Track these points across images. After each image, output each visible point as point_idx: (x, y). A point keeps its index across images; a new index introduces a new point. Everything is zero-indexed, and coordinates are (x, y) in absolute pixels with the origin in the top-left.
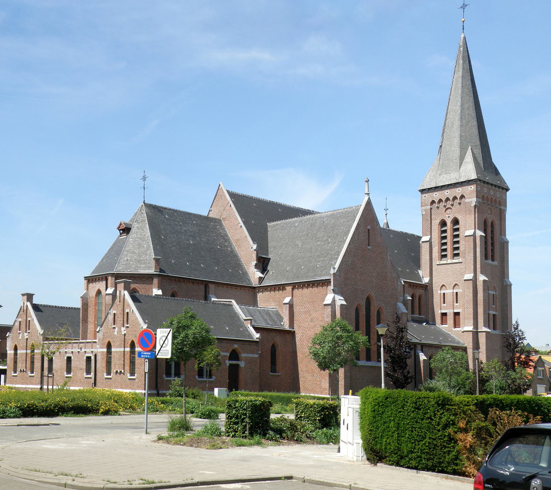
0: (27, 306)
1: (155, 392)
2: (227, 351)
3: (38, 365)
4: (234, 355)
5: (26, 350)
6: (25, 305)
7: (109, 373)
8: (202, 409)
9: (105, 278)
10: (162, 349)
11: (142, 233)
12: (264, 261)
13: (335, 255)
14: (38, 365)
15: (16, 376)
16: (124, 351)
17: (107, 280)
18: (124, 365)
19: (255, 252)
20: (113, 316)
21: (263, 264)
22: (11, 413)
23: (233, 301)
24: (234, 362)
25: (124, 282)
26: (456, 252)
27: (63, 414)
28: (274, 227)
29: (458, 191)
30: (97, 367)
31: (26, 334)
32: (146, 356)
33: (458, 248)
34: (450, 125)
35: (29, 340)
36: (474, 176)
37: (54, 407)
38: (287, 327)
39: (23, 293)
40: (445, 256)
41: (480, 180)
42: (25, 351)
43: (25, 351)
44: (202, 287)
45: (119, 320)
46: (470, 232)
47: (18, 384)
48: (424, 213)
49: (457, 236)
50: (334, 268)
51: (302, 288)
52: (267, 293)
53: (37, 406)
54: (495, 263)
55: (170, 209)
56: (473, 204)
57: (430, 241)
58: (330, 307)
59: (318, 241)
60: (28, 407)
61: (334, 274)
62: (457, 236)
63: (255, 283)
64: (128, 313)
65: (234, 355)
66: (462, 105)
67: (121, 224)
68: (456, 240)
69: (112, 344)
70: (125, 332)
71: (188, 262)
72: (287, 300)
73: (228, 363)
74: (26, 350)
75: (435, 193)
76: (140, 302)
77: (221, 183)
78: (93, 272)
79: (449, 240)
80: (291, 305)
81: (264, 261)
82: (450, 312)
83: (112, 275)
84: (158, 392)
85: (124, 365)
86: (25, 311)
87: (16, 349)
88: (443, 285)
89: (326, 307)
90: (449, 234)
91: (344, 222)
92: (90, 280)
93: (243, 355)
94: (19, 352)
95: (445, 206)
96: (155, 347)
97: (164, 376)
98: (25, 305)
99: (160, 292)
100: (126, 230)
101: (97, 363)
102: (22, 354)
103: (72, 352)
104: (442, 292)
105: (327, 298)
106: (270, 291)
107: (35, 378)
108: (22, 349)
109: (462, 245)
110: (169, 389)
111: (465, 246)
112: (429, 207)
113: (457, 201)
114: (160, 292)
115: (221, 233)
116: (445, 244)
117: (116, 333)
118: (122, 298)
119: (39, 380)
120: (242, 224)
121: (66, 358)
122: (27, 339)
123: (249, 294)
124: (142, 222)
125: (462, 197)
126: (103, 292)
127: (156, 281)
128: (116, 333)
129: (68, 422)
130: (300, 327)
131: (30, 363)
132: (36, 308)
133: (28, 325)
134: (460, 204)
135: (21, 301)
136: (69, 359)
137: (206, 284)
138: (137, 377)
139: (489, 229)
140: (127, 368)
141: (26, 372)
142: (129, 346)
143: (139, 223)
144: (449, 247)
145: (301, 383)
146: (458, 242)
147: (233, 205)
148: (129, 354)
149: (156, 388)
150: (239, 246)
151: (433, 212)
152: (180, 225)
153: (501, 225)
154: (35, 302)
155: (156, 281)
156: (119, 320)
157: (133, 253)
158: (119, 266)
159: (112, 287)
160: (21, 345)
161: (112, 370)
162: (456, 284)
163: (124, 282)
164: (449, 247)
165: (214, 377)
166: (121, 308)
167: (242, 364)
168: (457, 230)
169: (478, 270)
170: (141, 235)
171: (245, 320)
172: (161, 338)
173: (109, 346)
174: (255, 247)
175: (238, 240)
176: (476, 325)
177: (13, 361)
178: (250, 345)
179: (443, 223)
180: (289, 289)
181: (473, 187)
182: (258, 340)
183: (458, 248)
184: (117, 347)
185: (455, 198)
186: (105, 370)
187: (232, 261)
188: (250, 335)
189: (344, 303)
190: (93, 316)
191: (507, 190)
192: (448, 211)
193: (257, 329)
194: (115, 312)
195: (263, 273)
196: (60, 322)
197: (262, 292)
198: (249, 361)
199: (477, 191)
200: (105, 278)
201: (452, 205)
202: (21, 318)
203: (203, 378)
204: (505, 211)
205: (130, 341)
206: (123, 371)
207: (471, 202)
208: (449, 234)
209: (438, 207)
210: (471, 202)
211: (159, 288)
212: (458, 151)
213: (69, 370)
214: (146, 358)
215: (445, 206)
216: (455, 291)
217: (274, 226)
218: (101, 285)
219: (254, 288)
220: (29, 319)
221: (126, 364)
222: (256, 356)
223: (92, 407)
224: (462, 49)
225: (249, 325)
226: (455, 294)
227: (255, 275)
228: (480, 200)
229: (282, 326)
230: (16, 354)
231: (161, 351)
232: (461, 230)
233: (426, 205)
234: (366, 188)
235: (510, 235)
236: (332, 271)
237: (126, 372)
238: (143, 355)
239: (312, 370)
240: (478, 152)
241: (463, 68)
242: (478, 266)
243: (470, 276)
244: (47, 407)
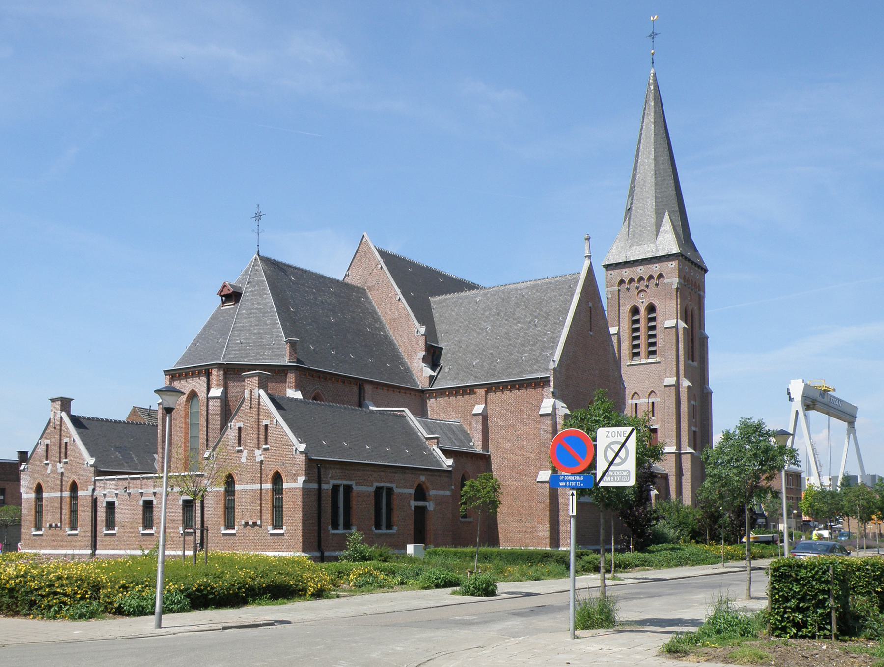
0: (61, 418)
1: (317, 554)
2: (411, 487)
3: (84, 515)
4: (421, 494)
5: (62, 491)
6: (58, 416)
7: (230, 525)
8: (467, 579)
9: (206, 372)
10: (612, 468)
11: (261, 299)
12: (434, 352)
13: (549, 342)
14: (84, 515)
15: (41, 535)
16: (261, 489)
17: (208, 375)
18: (261, 512)
19: (423, 338)
20: (236, 433)
21: (433, 357)
22: (173, 603)
23: (406, 410)
24: (421, 504)
25: (259, 375)
26: (652, 349)
27: (254, 601)
28: (441, 303)
29: (655, 269)
30: (206, 517)
31: (59, 465)
32: (573, 484)
33: (654, 344)
34: (642, 183)
35: (66, 475)
36: (675, 249)
37: (239, 589)
38: (479, 449)
39: (54, 397)
40: (638, 354)
41: (682, 256)
42: (59, 494)
43: (59, 494)
44: (355, 389)
45: (250, 437)
46: (670, 323)
47: (45, 548)
48: (610, 296)
49: (654, 328)
50: (554, 361)
51: (502, 391)
52: (443, 400)
53: (212, 588)
54: (695, 364)
55: (295, 268)
56: (675, 286)
57: (618, 334)
58: (549, 418)
59: (519, 322)
60: (197, 590)
61: (555, 369)
62: (654, 328)
63: (422, 383)
64: (266, 426)
65: (421, 494)
66: (655, 159)
67: (225, 286)
68: (651, 332)
69: (236, 478)
70: (262, 458)
71: (333, 349)
72: (479, 409)
73: (413, 504)
74: (62, 491)
75: (624, 270)
76: (284, 409)
77: (365, 234)
78: (179, 363)
79: (643, 333)
80: (484, 416)
81: (434, 352)
83: (220, 366)
84: (322, 554)
85: (261, 512)
86: (58, 428)
87: (39, 489)
88: (636, 393)
89: (543, 418)
90: (642, 325)
91: (555, 296)
92: (174, 375)
93: (432, 492)
94: (45, 495)
95: (637, 288)
96: (593, 465)
97: (330, 527)
98: (58, 416)
99: (298, 395)
100: (232, 296)
101: (206, 510)
102: (52, 498)
103: (155, 493)
104: (634, 402)
105: (543, 405)
106: (449, 396)
107: (79, 538)
108: (53, 489)
109: (660, 340)
110: (343, 547)
111: (663, 340)
112: (616, 288)
113: (655, 281)
114: (298, 395)
115: (368, 309)
116: (638, 338)
117: (243, 460)
118: (255, 402)
119: (88, 540)
120: (401, 296)
121: (141, 503)
122: (62, 473)
123: (419, 399)
124: (258, 284)
125: (661, 276)
126: (202, 395)
127: (291, 377)
128: (243, 460)
129: (308, 616)
130: (497, 449)
131: (68, 513)
132: (77, 422)
133: (64, 450)
134: (657, 285)
135: (50, 411)
136: (148, 506)
137: (361, 384)
138: (287, 532)
139: (689, 318)
140: (267, 516)
141: (61, 528)
142: (269, 481)
143: (254, 286)
144: (643, 342)
145: (500, 531)
146: (654, 336)
147: (385, 267)
148: (270, 493)
149: (320, 548)
150: (396, 329)
151: (621, 296)
152: (314, 293)
153: (700, 320)
154: (73, 413)
155: (291, 377)
156: (250, 437)
157: (249, 331)
158: (229, 353)
159: (218, 386)
160: (51, 484)
161: (237, 520)
162: (652, 392)
163: (259, 375)
164: (643, 342)
165: (395, 528)
166: (252, 419)
167: (430, 506)
168: (654, 319)
169: (682, 372)
170: (259, 303)
171: (427, 439)
172: (609, 446)
173: (230, 482)
174: (423, 330)
175: (394, 320)
176: (679, 447)
177: (33, 511)
178: (440, 476)
179: (635, 311)
180: (481, 392)
181: (674, 264)
182: (450, 469)
183: (654, 344)
184: (247, 483)
185: (651, 277)
186: (222, 522)
187: (384, 349)
188: (437, 462)
189: (568, 412)
190: (182, 435)
191: (706, 271)
192: (642, 294)
193: (447, 453)
194: (241, 425)
195: (433, 369)
196: (122, 445)
197: (436, 398)
198: (440, 501)
199: (679, 270)
200: (206, 372)
201: (647, 286)
202: (50, 439)
203: (380, 529)
204: (704, 297)
205: (272, 473)
206: (259, 522)
207: (672, 283)
208: (642, 325)
209: (628, 289)
210: (672, 283)
211: (297, 388)
212: (653, 217)
213: (148, 522)
214: (572, 488)
215: (637, 288)
216: (651, 400)
217: (441, 302)
218: (198, 384)
219: (423, 391)
220: (65, 440)
221: (264, 510)
222: (448, 493)
223: (297, 585)
224: (652, 88)
225: (435, 447)
226: (650, 404)
227: (422, 373)
228: (682, 281)
229: (472, 447)
230: (39, 498)
231: (610, 473)
232: (659, 319)
233: (612, 286)
234: (587, 248)
235: (709, 330)
236: (552, 366)
237: (264, 524)
238: (564, 481)
239: (519, 511)
240: (677, 218)
241: (655, 112)
242: (682, 368)
243: (672, 380)
244: (229, 589)
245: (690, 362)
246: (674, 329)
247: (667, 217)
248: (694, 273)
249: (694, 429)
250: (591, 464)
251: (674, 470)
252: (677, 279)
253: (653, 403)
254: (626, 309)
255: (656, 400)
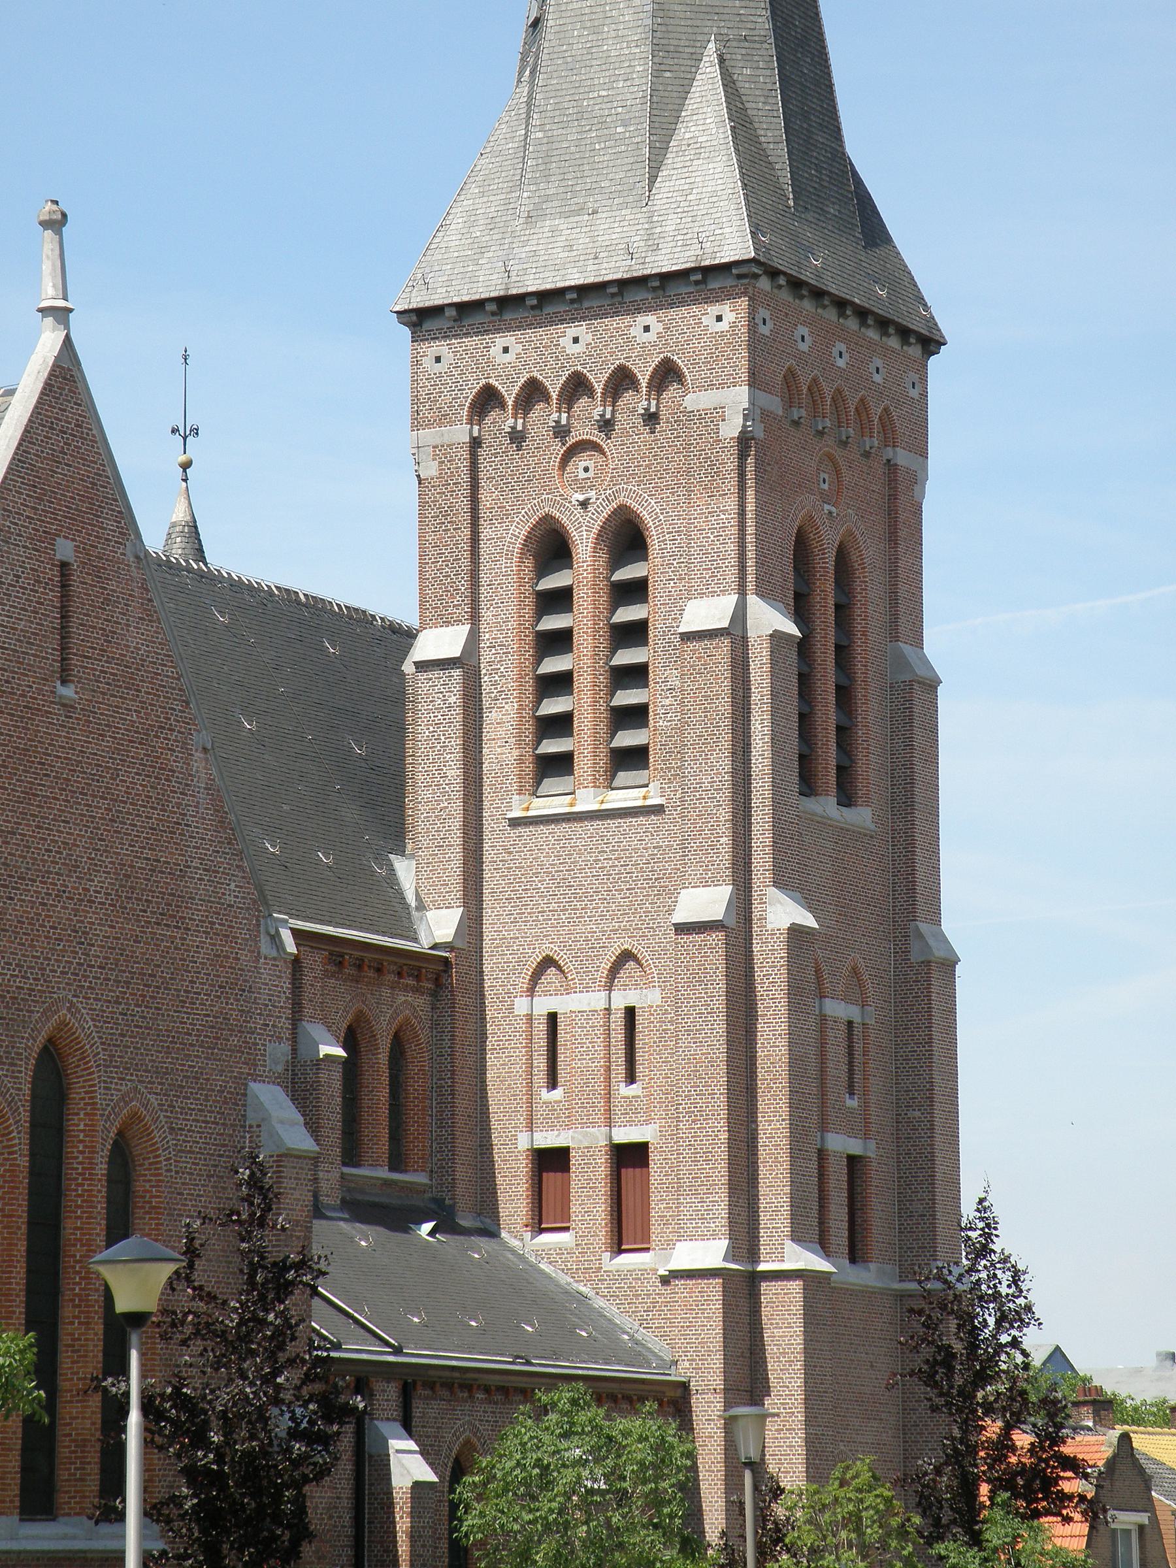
29: (643, 336)
36: (735, 244)
40: (561, 764)
46: (709, 611)
48: (430, 470)
49: (635, 633)
54: (862, 816)
56: (732, 428)
57: (467, 664)
75: (501, 341)
82: (588, 1142)
88: (548, 962)
95: (561, 432)
104: (543, 1005)
111: (683, 699)
112: (460, 433)
113: (636, 402)
144: (584, 703)
146: (637, 675)
151: (486, 469)
153: (893, 599)
162: (626, 956)
164: (584, 703)
168: (636, 591)
176: (745, 1234)
179: (551, 547)
181: (725, 319)
183: (636, 715)
191: (931, 343)
192: (583, 461)
199: (756, 344)
201: (606, 425)
204: (917, 479)
207: (718, 414)
208: (584, 619)
209: (517, 437)
215: (561, 432)
216: (620, 1000)
226: (618, 1021)
228: (774, 404)
233: (443, 419)
234: (48, 267)
243: (708, 901)
245: (827, 806)
246: (722, 649)
247: (708, 76)
248: (844, 355)
249: (841, 1144)
250: (54, 1372)
251: (716, 1362)
252: (739, 396)
253: (553, 1018)
254: (505, 539)
255: (646, 997)
